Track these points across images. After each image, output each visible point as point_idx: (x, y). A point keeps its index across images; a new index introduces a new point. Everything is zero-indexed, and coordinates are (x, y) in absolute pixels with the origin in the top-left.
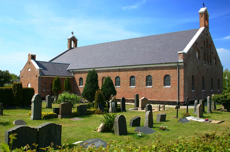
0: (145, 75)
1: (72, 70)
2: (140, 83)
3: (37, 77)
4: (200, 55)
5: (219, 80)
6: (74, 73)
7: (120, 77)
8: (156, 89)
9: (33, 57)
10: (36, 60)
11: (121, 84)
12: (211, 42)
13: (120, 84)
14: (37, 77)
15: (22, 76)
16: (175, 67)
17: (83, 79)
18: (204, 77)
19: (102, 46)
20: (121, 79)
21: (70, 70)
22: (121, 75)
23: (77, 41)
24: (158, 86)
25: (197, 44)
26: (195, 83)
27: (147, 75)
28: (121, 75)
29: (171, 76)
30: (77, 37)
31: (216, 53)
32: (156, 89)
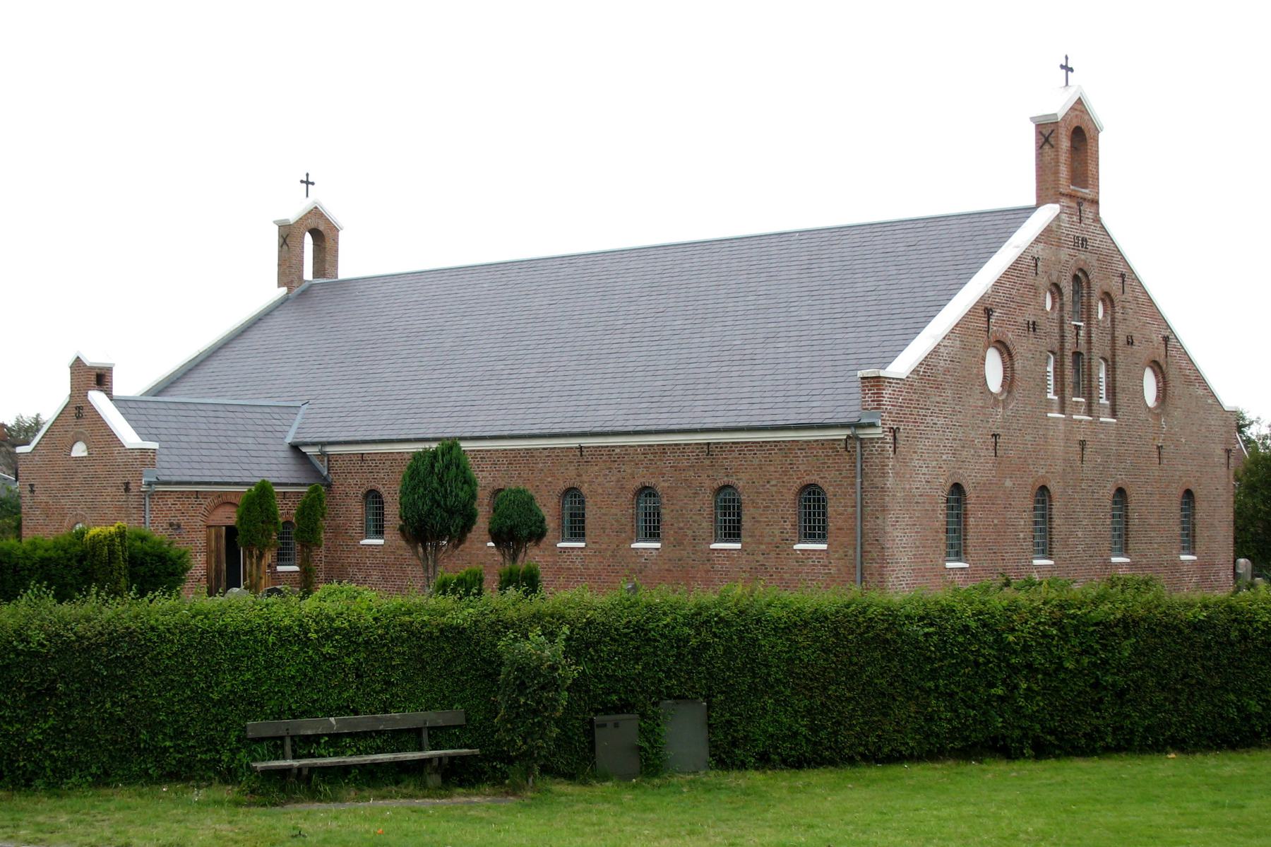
0: (707, 483)
1: (323, 444)
2: (682, 525)
3: (127, 490)
4: (1013, 369)
5: (1188, 494)
6: (329, 461)
7: (585, 489)
8: (761, 558)
9: (101, 378)
10: (117, 392)
11: (587, 532)
12: (1123, 276)
13: (584, 529)
14: (127, 490)
15: (32, 486)
16: (846, 448)
17: (387, 498)
18: (1054, 487)
19: (271, 694)
20: (589, 504)
21: (306, 444)
22: (591, 482)
23: (341, 234)
24: (767, 540)
25: (988, 312)
26: (971, 521)
27: (716, 486)
28: (591, 482)
29: (829, 490)
30: (334, 212)
31: (1166, 339)
32: (761, 558)
